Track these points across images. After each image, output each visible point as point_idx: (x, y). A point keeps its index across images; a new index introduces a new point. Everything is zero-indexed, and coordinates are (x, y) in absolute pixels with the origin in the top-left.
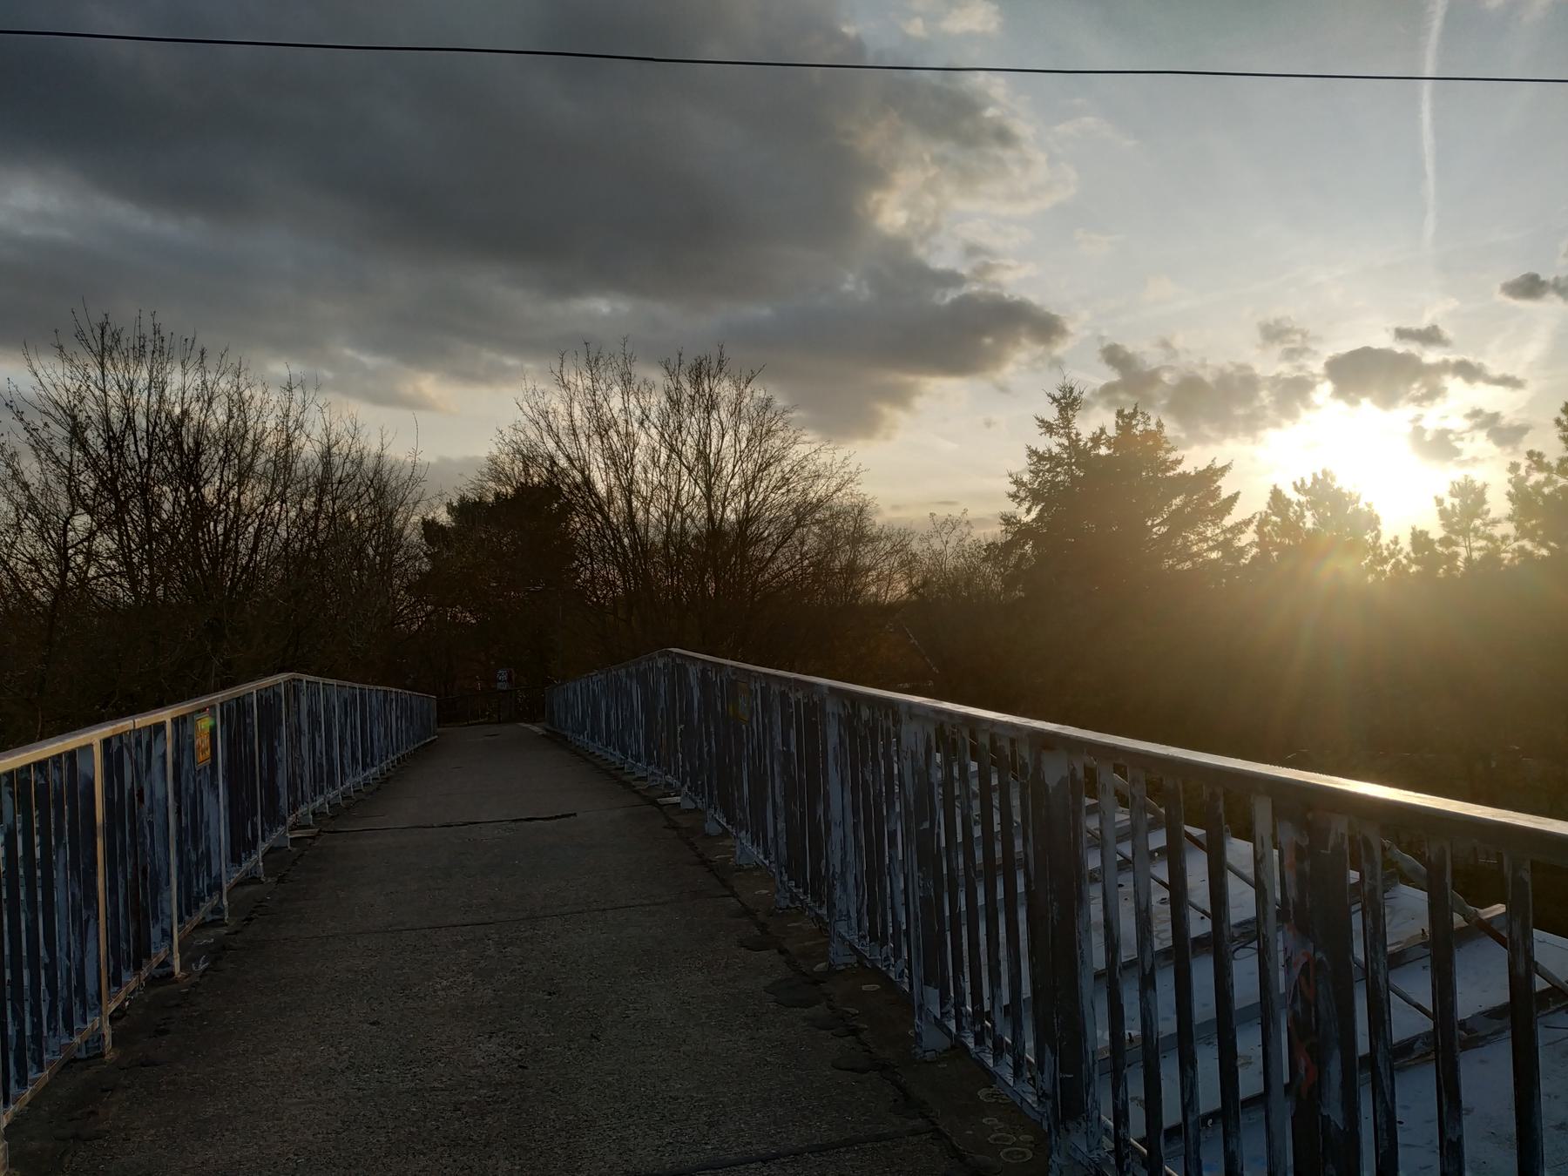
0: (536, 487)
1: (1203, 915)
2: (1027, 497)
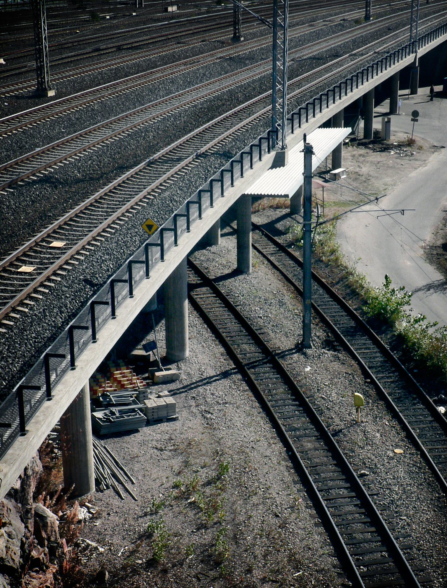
0: (387, 548)
2: (92, 513)
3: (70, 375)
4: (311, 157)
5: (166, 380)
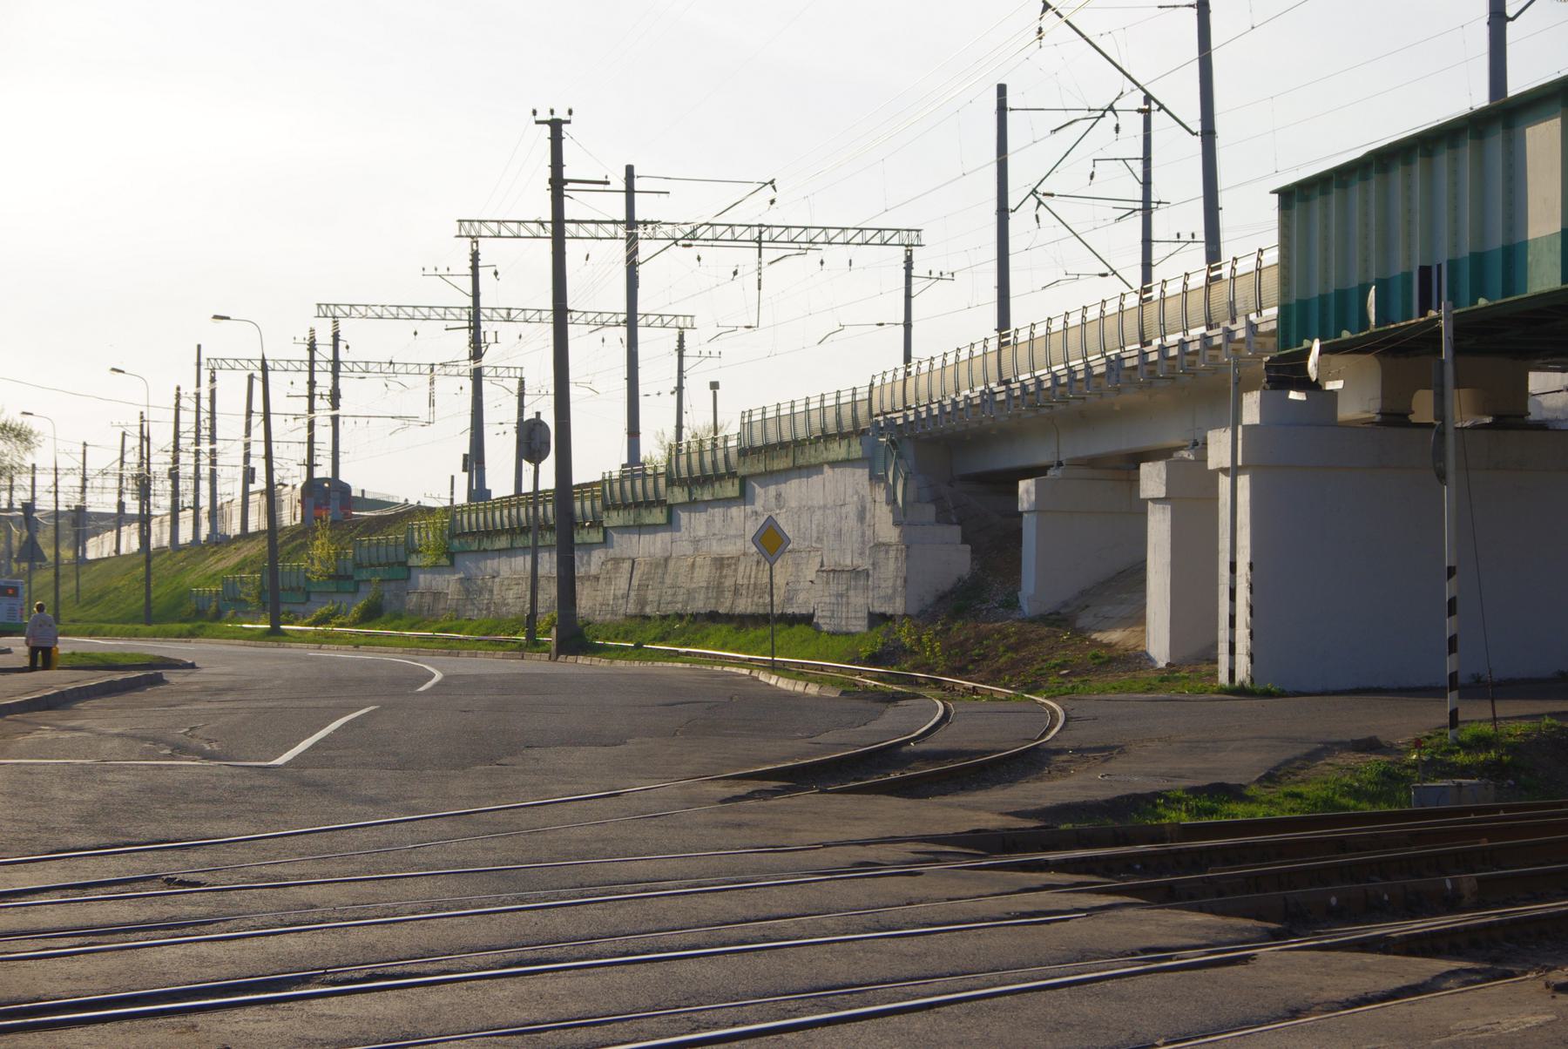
1: (367, 419)
3: (1248, 560)
4: (1138, 468)
5: (13, 1000)
